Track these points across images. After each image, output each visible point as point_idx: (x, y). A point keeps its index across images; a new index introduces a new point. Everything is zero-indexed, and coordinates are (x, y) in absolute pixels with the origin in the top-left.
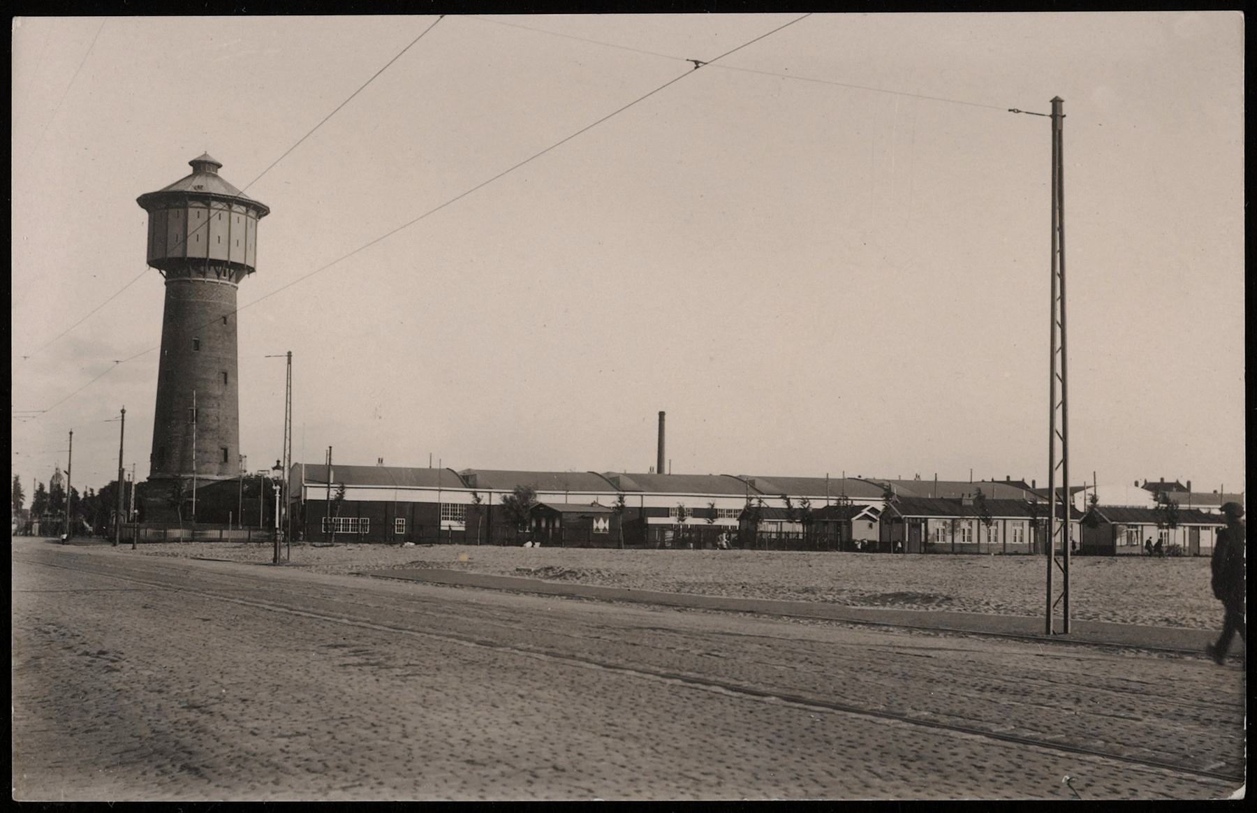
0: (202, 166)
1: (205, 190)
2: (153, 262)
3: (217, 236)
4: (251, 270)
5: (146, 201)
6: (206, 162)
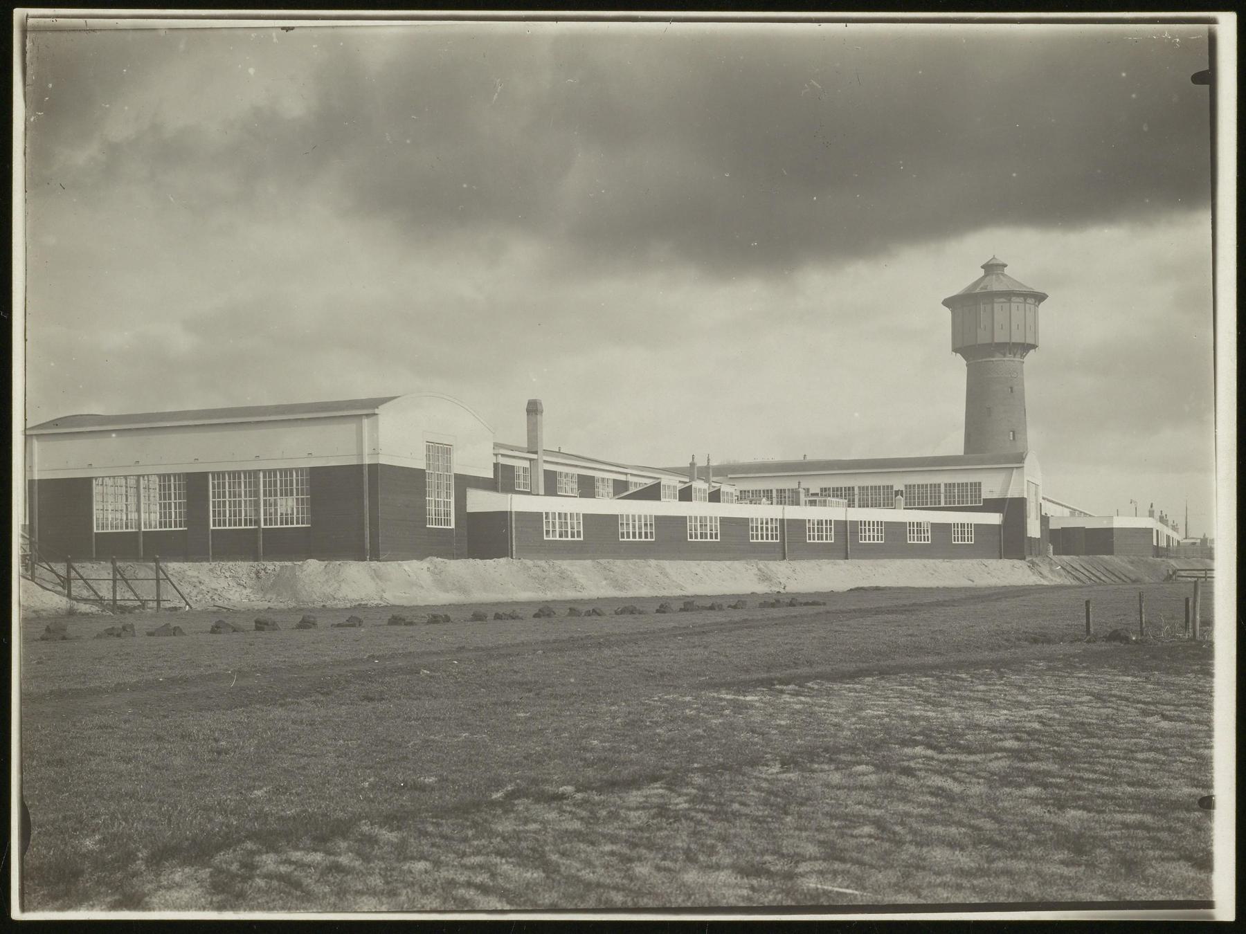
0: (992, 268)
1: (989, 289)
2: (955, 350)
3: (1005, 322)
4: (1034, 347)
5: (947, 303)
6: (992, 265)
